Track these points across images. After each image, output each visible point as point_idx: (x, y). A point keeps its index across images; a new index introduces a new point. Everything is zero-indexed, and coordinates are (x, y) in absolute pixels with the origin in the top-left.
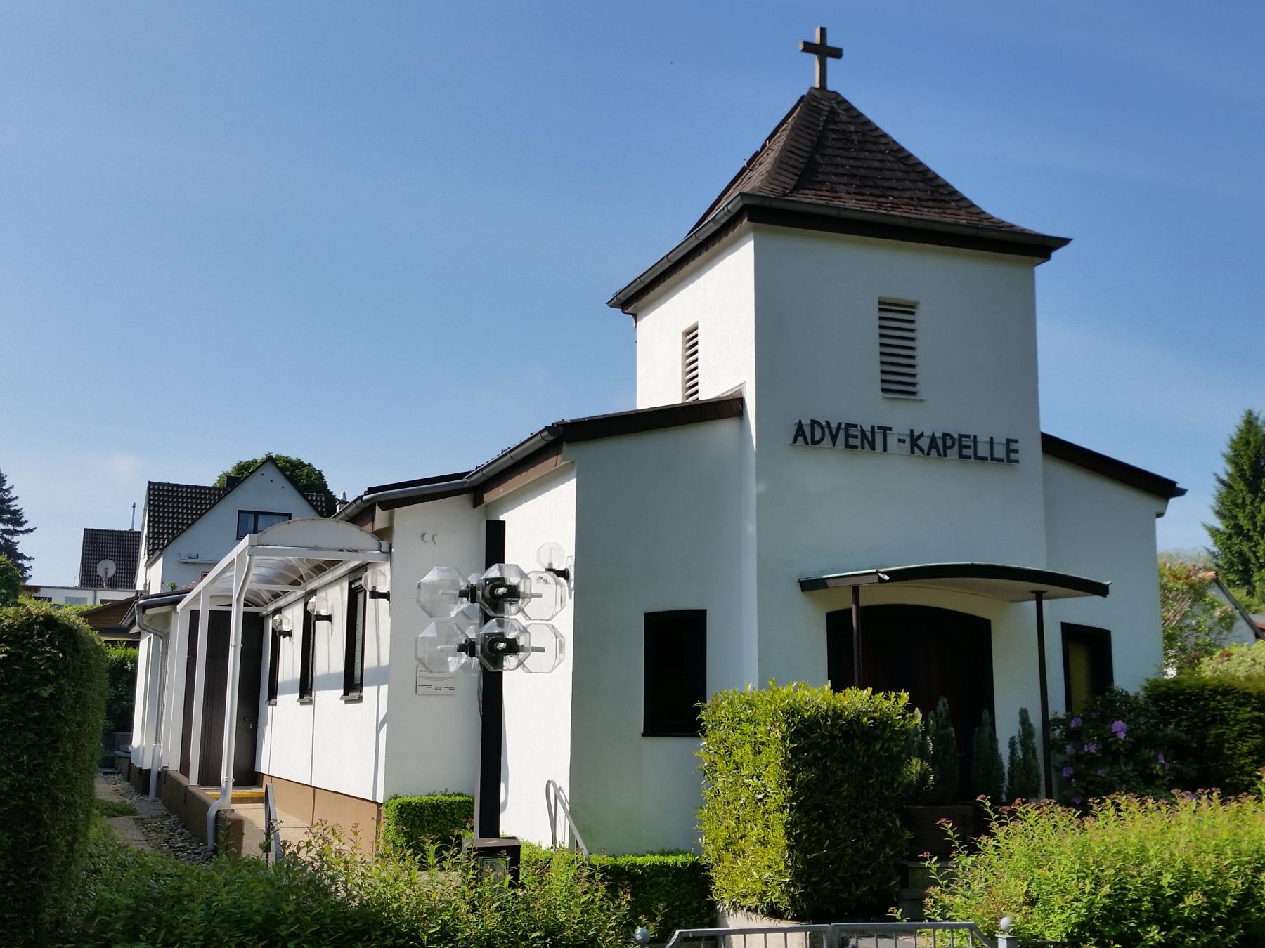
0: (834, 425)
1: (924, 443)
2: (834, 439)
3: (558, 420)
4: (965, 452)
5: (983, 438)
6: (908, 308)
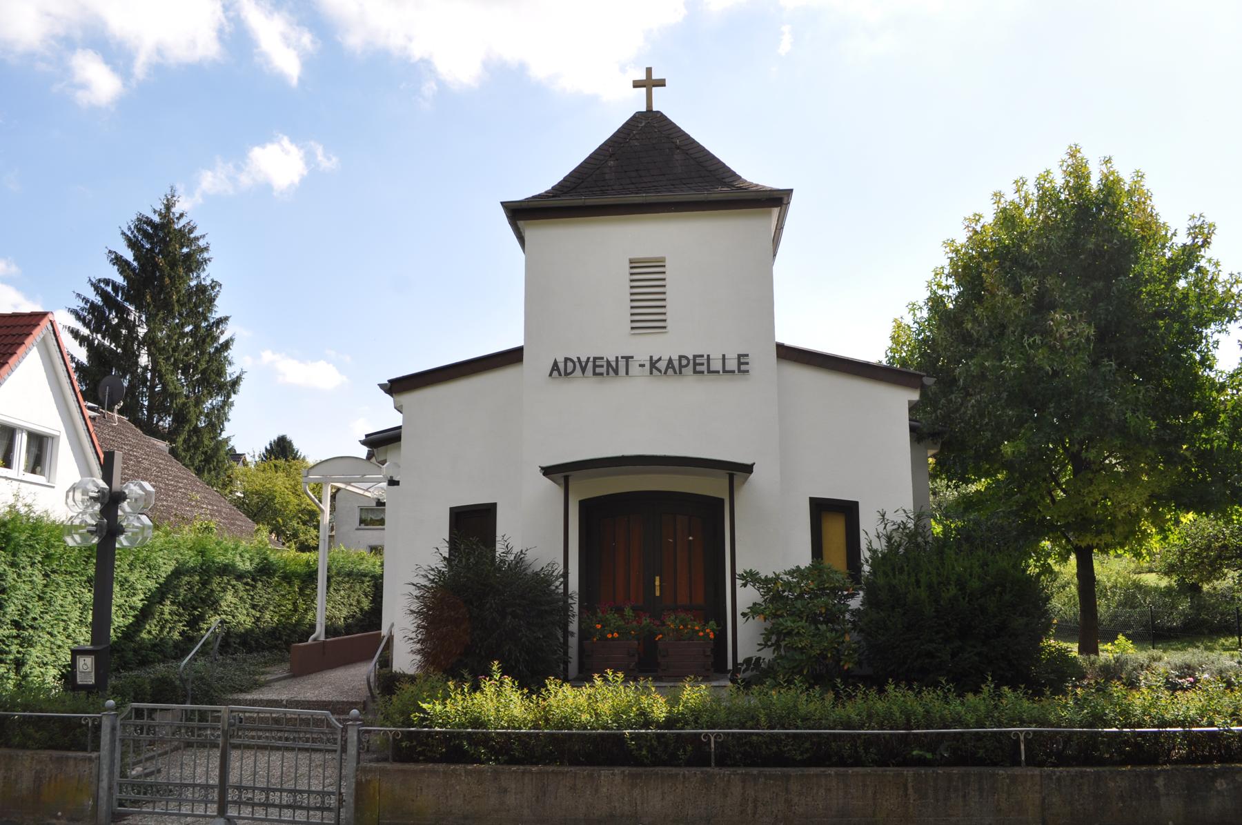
0: (584, 359)
1: (662, 365)
2: (583, 370)
6: (659, 263)
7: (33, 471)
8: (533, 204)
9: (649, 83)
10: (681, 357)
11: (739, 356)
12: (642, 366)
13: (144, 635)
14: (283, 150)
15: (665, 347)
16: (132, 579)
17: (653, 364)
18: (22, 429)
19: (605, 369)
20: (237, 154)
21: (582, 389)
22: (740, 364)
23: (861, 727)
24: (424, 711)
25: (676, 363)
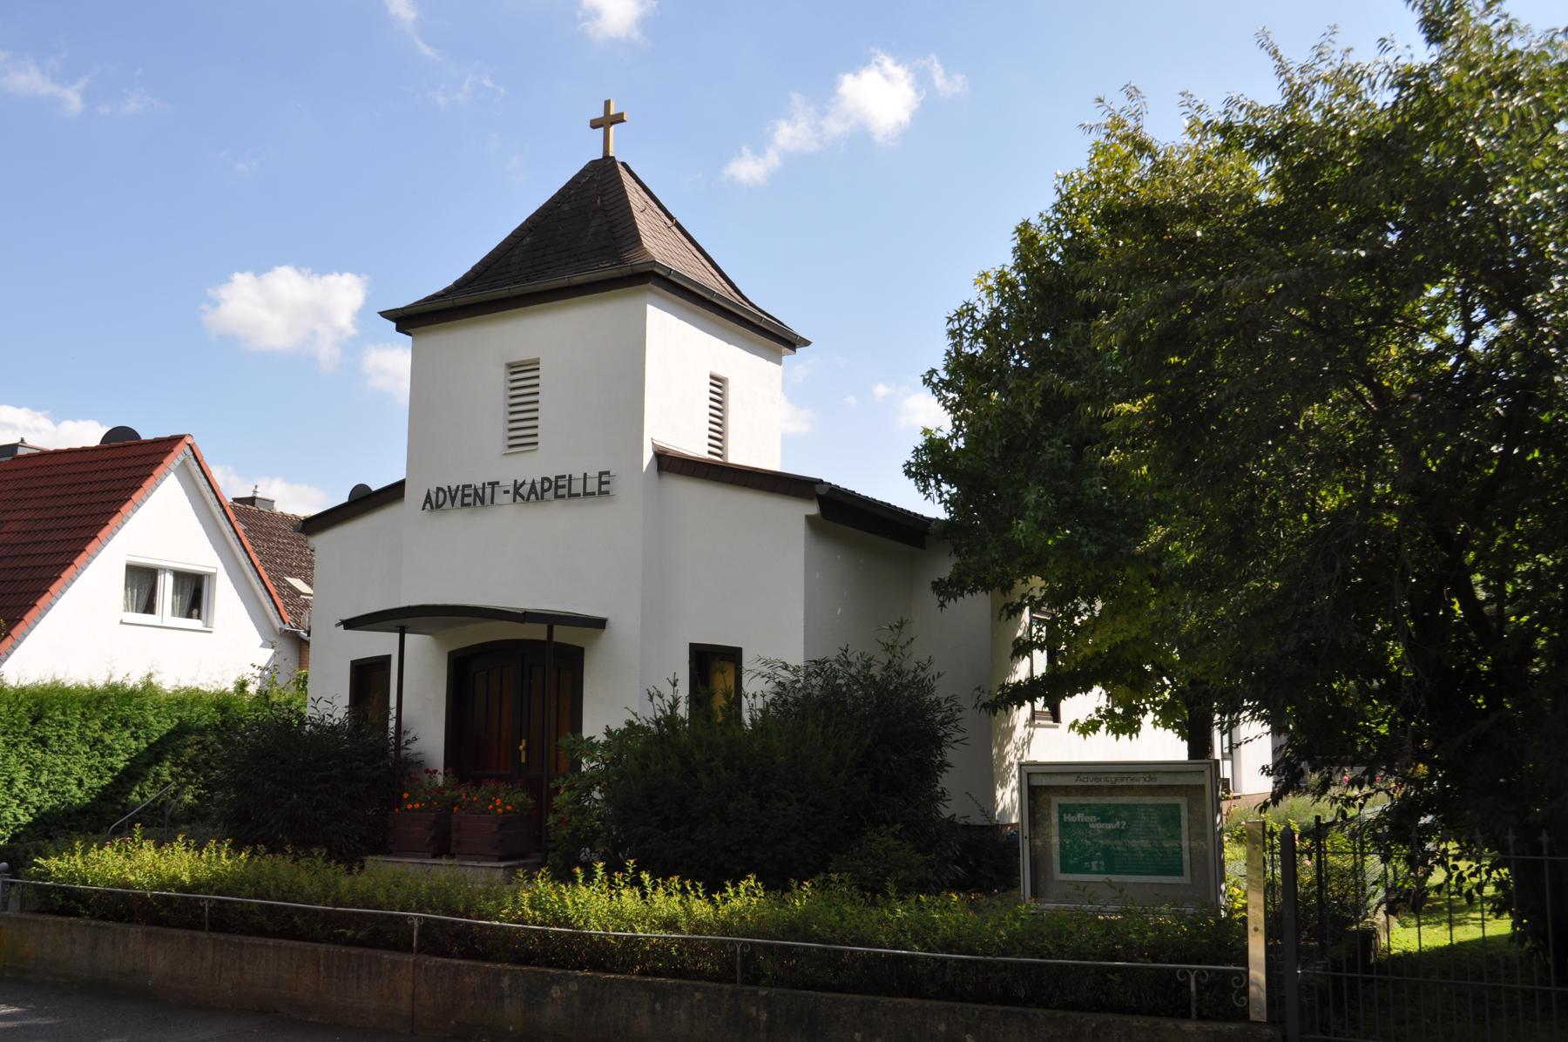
0: (454, 487)
1: (525, 490)
2: (453, 499)
3: (194, 684)
4: (560, 492)
5: (578, 475)
6: (532, 366)
7: (189, 616)
8: (447, 303)
9: (607, 121)
10: (544, 479)
11: (601, 474)
12: (507, 492)
13: (134, 797)
14: (887, 77)
15: (530, 468)
16: (108, 739)
17: (517, 488)
18: (165, 570)
19: (474, 497)
20: (823, 92)
21: (456, 521)
22: (601, 483)
23: (318, 903)
24: (40, 866)
25: (538, 487)
